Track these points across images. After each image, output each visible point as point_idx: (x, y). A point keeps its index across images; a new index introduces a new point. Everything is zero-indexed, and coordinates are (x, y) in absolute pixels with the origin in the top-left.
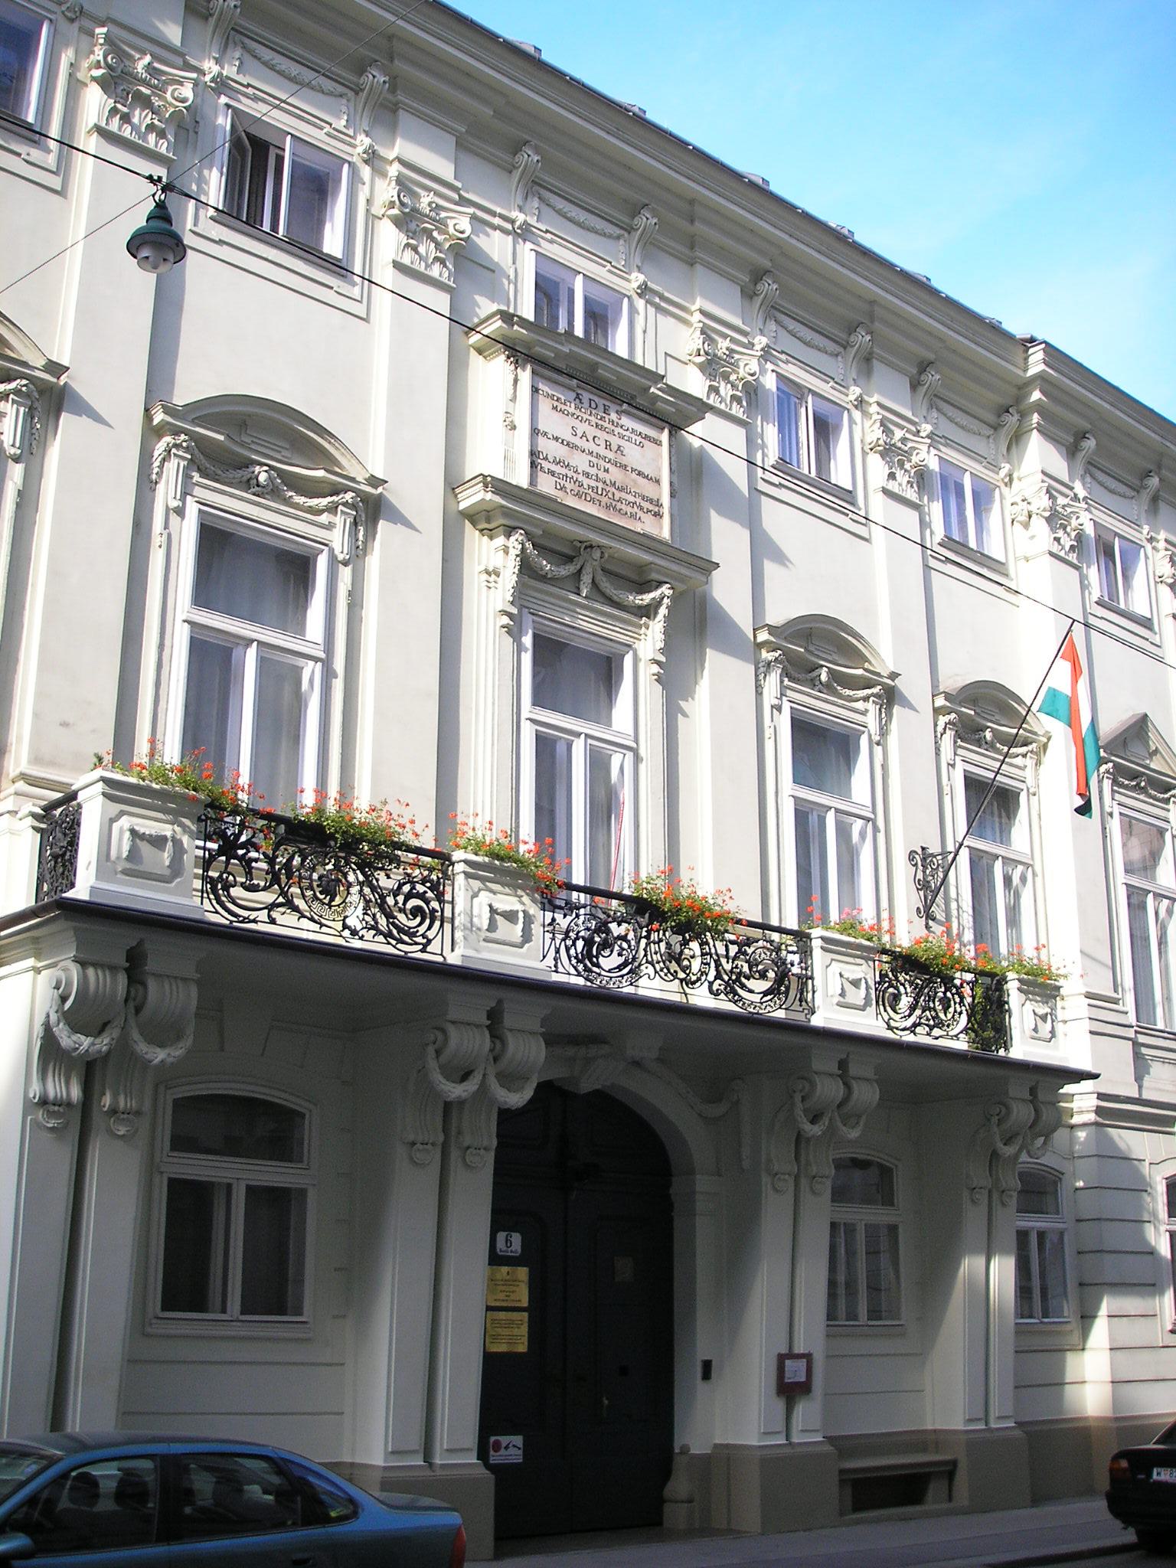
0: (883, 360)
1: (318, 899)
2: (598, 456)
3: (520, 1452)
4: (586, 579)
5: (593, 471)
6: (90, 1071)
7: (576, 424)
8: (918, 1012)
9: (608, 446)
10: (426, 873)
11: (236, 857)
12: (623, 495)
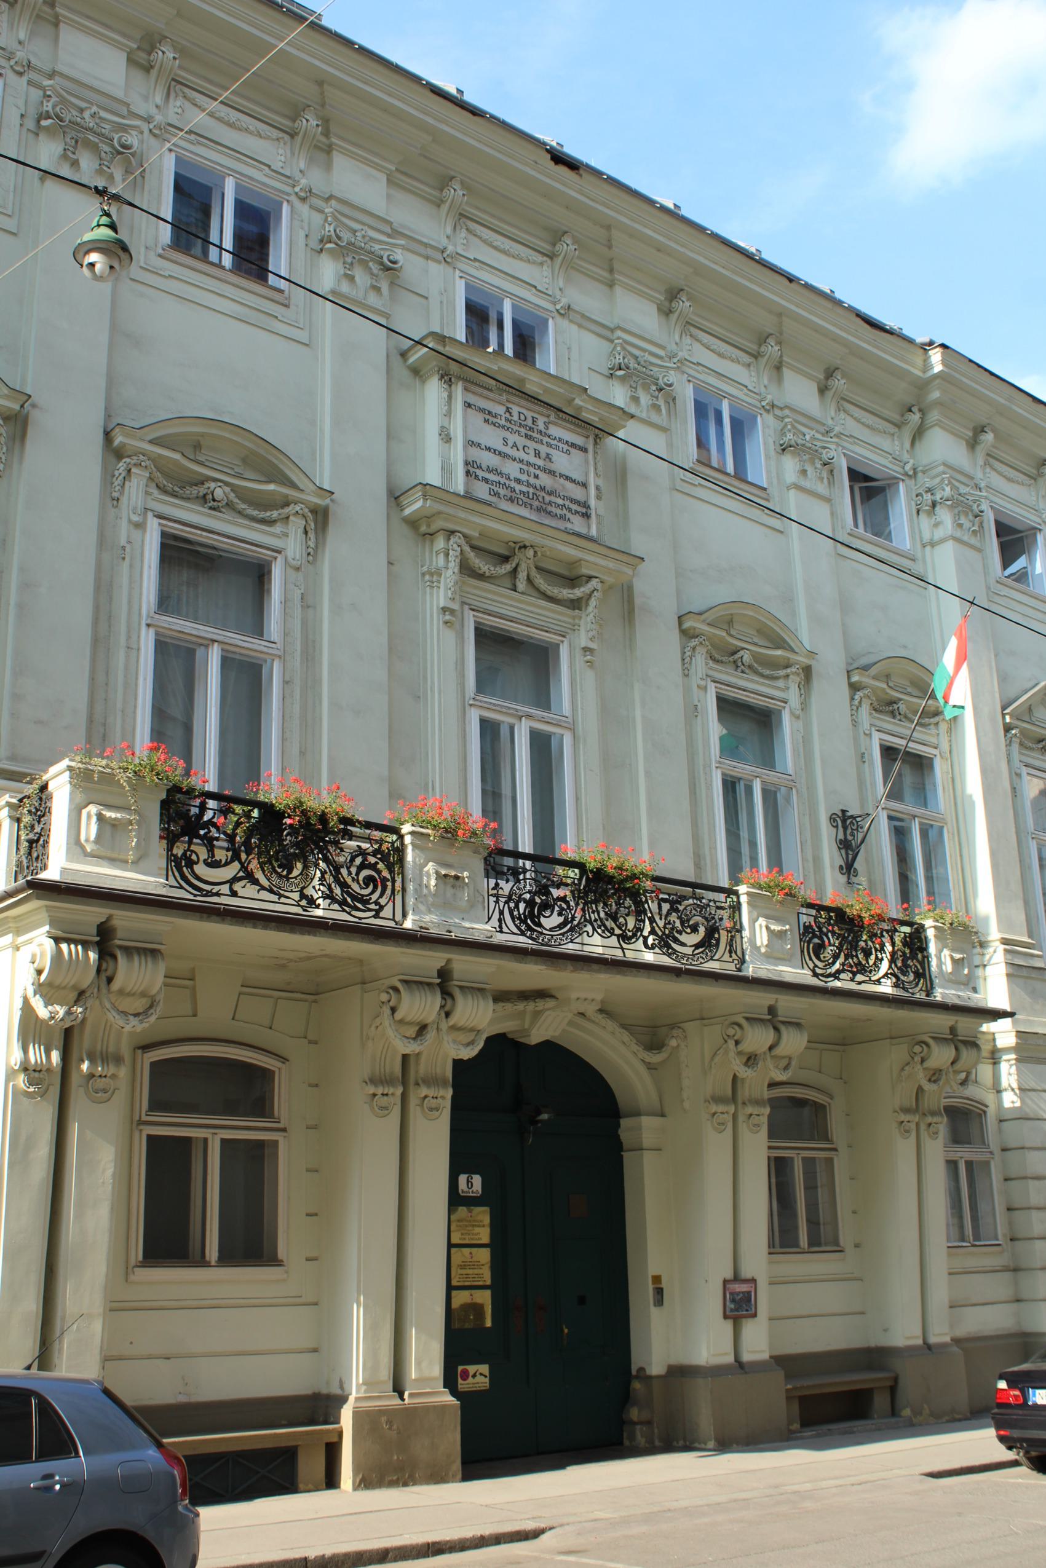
0: (793, 368)
1: (276, 872)
2: (529, 464)
3: (487, 1380)
4: (522, 575)
5: (524, 477)
6: (67, 1038)
7: (507, 434)
8: (841, 959)
9: (537, 454)
10: (376, 846)
11: (199, 837)
12: (553, 499)
